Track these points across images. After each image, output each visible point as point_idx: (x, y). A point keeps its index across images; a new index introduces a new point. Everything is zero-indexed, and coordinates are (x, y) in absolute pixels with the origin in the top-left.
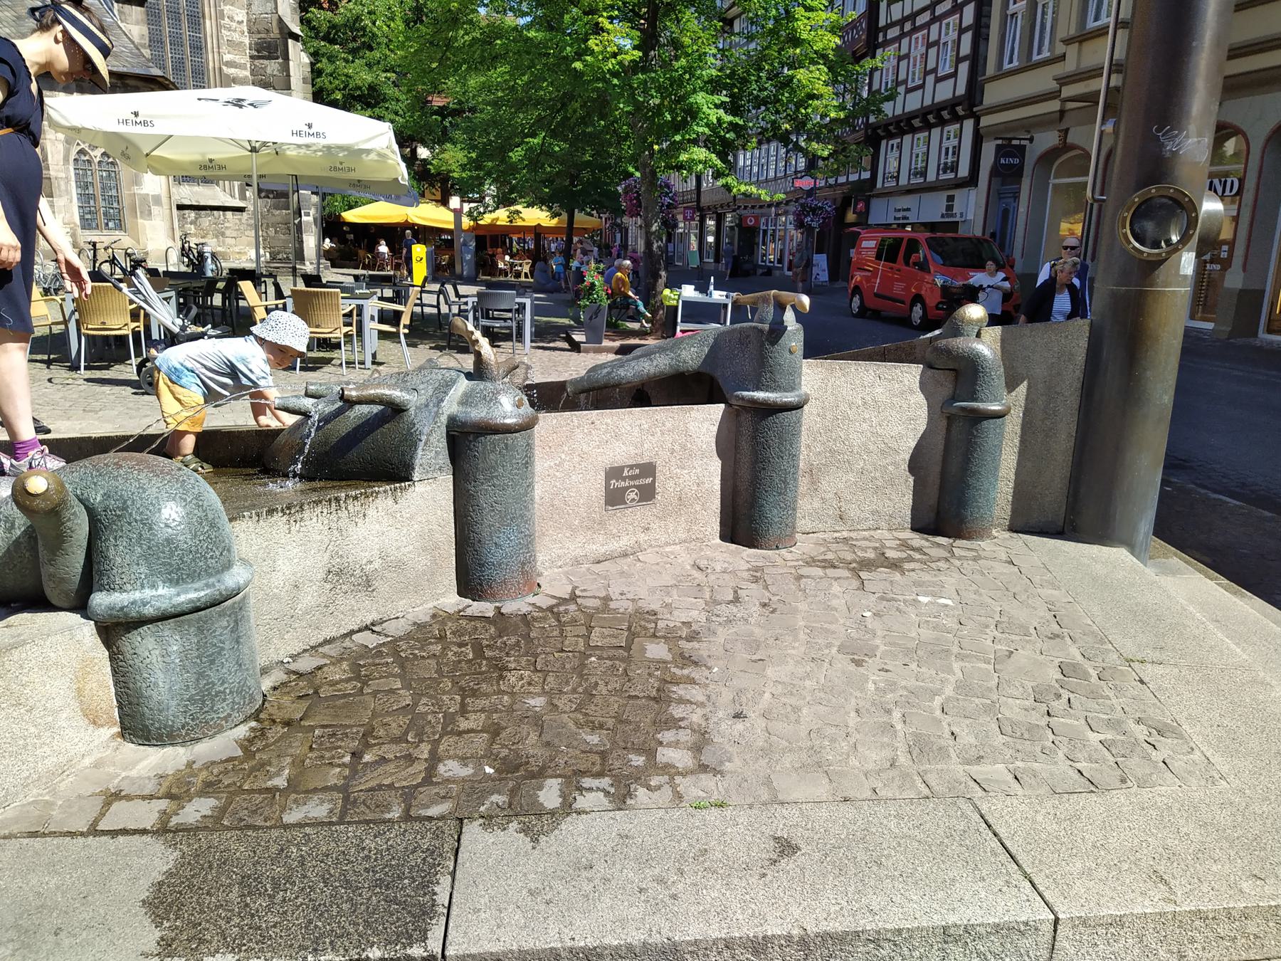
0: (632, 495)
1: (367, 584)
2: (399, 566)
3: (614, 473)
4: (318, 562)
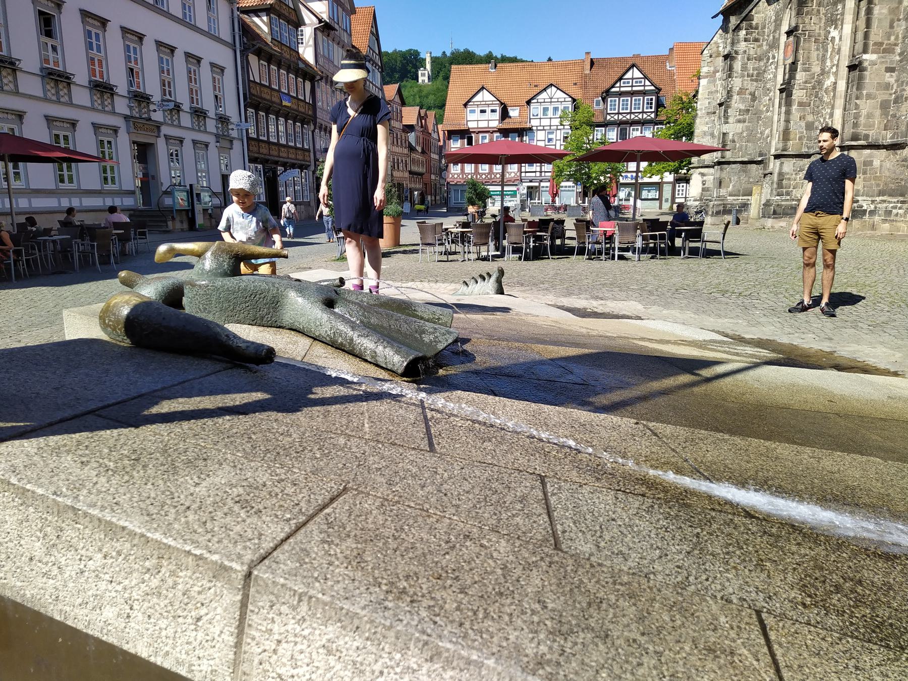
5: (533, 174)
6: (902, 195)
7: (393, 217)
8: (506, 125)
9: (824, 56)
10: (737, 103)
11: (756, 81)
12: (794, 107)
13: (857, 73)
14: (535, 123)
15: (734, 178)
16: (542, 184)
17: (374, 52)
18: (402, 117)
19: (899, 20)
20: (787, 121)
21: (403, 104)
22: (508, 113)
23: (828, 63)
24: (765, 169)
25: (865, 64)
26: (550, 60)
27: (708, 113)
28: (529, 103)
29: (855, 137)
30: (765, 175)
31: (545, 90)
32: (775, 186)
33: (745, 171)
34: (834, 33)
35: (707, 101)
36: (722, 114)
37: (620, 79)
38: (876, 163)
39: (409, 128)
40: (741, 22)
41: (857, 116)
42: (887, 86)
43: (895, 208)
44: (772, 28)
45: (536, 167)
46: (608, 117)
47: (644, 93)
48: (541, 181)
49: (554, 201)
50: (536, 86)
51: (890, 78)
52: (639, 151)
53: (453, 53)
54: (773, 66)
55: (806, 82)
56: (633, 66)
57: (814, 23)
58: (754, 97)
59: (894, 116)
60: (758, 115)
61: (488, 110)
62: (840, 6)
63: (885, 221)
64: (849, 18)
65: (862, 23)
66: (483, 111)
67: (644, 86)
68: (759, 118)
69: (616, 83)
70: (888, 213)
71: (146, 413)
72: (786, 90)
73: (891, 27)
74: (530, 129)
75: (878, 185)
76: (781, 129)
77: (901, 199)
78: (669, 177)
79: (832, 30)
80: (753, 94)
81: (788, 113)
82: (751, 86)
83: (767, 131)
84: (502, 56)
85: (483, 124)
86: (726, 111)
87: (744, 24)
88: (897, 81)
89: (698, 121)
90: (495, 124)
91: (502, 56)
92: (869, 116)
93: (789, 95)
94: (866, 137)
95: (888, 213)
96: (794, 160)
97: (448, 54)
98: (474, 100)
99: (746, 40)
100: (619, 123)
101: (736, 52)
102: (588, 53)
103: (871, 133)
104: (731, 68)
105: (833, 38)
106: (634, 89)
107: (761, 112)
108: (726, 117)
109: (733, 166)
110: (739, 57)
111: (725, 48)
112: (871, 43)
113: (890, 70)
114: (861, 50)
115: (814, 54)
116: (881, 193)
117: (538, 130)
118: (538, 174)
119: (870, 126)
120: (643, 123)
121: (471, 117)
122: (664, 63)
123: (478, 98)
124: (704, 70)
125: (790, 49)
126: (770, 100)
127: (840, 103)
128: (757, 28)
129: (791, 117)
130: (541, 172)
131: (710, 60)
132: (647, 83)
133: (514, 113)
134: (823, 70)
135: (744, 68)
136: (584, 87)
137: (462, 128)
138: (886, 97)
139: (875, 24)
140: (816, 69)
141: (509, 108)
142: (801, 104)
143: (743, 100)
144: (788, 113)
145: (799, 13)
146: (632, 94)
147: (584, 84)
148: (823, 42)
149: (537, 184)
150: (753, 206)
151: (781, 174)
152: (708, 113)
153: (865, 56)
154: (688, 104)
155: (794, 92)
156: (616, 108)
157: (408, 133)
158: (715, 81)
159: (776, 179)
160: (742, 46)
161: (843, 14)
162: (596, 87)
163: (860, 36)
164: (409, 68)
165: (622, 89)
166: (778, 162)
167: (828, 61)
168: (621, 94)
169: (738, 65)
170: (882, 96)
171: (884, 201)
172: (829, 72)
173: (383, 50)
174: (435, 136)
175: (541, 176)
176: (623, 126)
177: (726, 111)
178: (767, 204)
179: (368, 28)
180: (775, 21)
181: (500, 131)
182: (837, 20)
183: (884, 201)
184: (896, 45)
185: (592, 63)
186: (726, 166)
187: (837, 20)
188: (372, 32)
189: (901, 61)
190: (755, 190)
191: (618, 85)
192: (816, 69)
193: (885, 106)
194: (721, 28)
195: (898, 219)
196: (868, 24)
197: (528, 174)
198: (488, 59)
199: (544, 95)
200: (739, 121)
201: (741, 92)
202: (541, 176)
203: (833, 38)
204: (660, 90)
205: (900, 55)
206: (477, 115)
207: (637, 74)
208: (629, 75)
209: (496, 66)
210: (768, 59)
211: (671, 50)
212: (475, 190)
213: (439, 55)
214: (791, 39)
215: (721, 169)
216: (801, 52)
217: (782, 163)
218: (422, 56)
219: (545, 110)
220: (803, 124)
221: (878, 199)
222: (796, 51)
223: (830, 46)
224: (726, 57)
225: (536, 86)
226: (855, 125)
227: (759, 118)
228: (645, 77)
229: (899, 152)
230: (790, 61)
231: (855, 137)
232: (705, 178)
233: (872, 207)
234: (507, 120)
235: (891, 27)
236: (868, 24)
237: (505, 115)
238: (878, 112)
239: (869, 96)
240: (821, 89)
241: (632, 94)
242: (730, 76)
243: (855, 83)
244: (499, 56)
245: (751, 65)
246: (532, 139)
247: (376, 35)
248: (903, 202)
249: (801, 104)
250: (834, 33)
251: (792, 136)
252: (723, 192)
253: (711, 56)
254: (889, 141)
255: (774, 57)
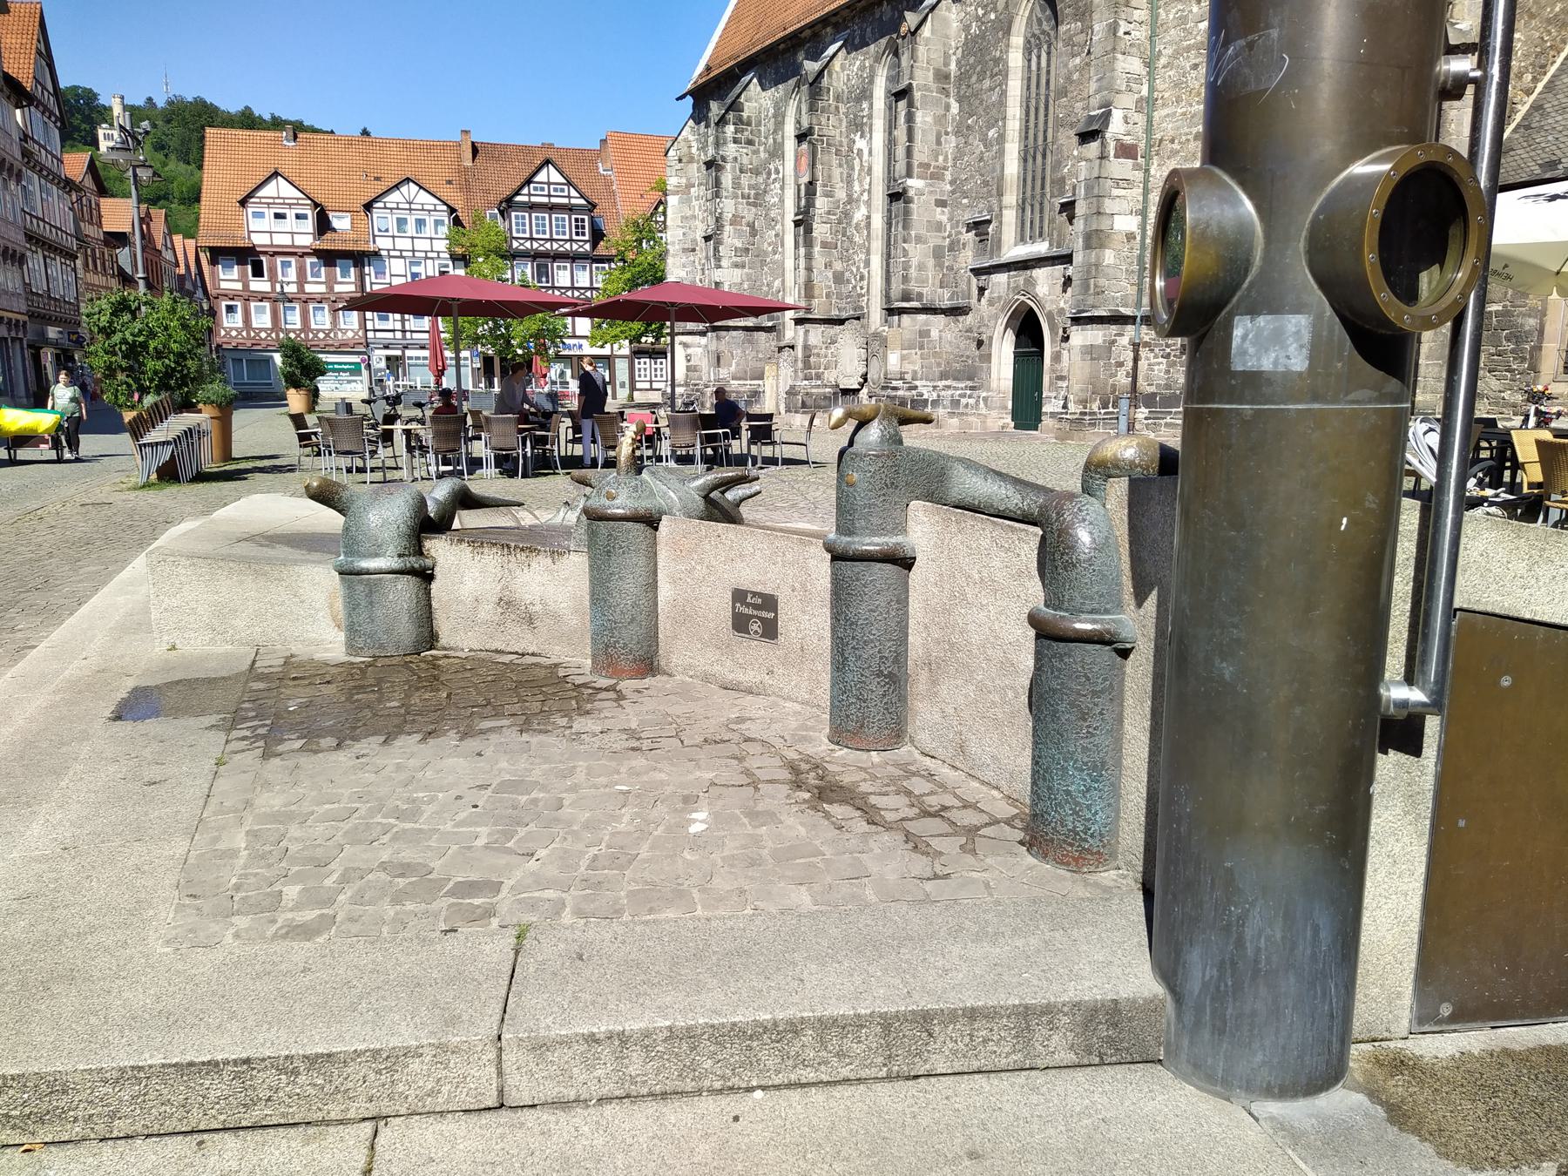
0: (755, 627)
1: (530, 620)
2: (556, 617)
3: (739, 595)
4: (492, 590)
5: (390, 335)
6: (971, 379)
7: (219, 406)
8: (326, 244)
9: (849, 176)
10: (731, 239)
11: (755, 205)
12: (817, 249)
13: (901, 204)
14: (383, 243)
15: (738, 352)
16: (408, 353)
17: (44, 88)
18: (100, 217)
19: (947, 133)
20: (809, 269)
21: (103, 191)
22: (329, 222)
23: (857, 187)
24: (779, 340)
25: (911, 193)
26: (365, 133)
27: (685, 250)
28: (368, 207)
29: (906, 297)
30: (780, 349)
31: (397, 187)
32: (800, 365)
33: (750, 342)
34: (860, 143)
35: (681, 232)
36: (711, 253)
37: (529, 182)
38: (934, 334)
39: (119, 239)
40: (727, 111)
41: (906, 267)
42: (939, 227)
43: (964, 396)
44: (771, 126)
45: (394, 321)
46: (515, 244)
47: (570, 209)
48: (406, 347)
49: (438, 383)
50: (377, 179)
51: (942, 215)
52: (673, 304)
53: (170, 103)
54: (777, 185)
55: (829, 213)
56: (547, 162)
57: (832, 126)
58: (754, 232)
59: (950, 268)
60: (761, 256)
61: (291, 214)
62: (865, 105)
63: (952, 414)
64: (879, 124)
65: (901, 133)
66: (278, 216)
67: (569, 197)
68: (763, 263)
69: (521, 188)
70: (955, 403)
71: (1155, 592)
72: (803, 222)
73: (939, 143)
74: (376, 254)
75: (939, 365)
76: (802, 280)
77: (970, 383)
78: (624, 348)
79: (857, 138)
80: (751, 226)
81: (809, 257)
82: (749, 214)
83: (777, 283)
84: (273, 117)
85: (282, 240)
86: (716, 249)
87: (731, 116)
88: (950, 220)
89: (670, 261)
90: (306, 241)
91: (273, 117)
92: (921, 267)
93: (809, 231)
94: (920, 296)
95: (955, 403)
96: (822, 327)
97: (161, 103)
98: (260, 194)
99: (735, 141)
100: (535, 256)
101: (724, 159)
102: (465, 132)
103: (925, 291)
104: (718, 183)
105: (860, 151)
106: (554, 200)
107: (766, 253)
108: (718, 259)
109: (734, 333)
110: (728, 166)
111: (703, 148)
112: (916, 163)
113: (941, 203)
114: (904, 173)
115: (836, 172)
116: (944, 376)
117: (390, 257)
118: (399, 335)
119: (923, 281)
120: (573, 258)
121: (255, 224)
122: (593, 162)
123: (269, 190)
124: (672, 182)
125: (805, 161)
126: (777, 235)
127: (877, 246)
128: (749, 124)
129: (814, 263)
130: (404, 331)
131: (679, 166)
132: (573, 193)
133: (341, 223)
134: (849, 196)
135: (737, 185)
136: (466, 188)
137: (241, 244)
138: (939, 242)
139: (918, 136)
140: (841, 195)
141: (331, 215)
142: (825, 245)
143: (739, 234)
144: (809, 257)
145: (812, 109)
146: (552, 208)
147: (465, 182)
148: (847, 155)
149: (398, 353)
150: (768, 394)
151: (806, 347)
152: (685, 250)
153: (910, 182)
154: (648, 229)
155: (815, 226)
156: (525, 230)
157: (115, 247)
158: (689, 200)
159: (800, 355)
160: (731, 150)
161: (870, 117)
162: (487, 192)
163: (900, 152)
164: (76, 122)
165: (534, 199)
166: (801, 329)
167: (856, 183)
168: (532, 207)
169: (727, 179)
170: (934, 240)
171: (949, 387)
172: (858, 200)
173: (63, 83)
174: (168, 255)
175: (404, 338)
176: (543, 260)
177: (716, 249)
178: (792, 392)
179: (31, 43)
180: (775, 116)
181: (318, 253)
182: (863, 124)
183: (949, 387)
184: (945, 168)
185: (475, 150)
186: (723, 333)
187: (863, 124)
188: (39, 52)
189: (953, 192)
190: (769, 370)
191: (525, 191)
192: (841, 195)
193: (938, 253)
194: (692, 117)
195: (968, 411)
196: (910, 138)
197: (379, 335)
198: (277, 124)
199: (395, 197)
200: (736, 266)
201: (736, 220)
202: (404, 338)
203: (860, 151)
204: (594, 206)
205: (951, 183)
206: (268, 222)
207: (556, 177)
208: (542, 177)
209: (295, 137)
210: (769, 174)
211: (604, 142)
212: (300, 360)
213: (140, 101)
214: (805, 146)
215: (718, 338)
216: (819, 167)
217: (807, 332)
218: (102, 101)
219: (401, 222)
220: (830, 275)
221: (941, 384)
222: (813, 165)
223: (857, 162)
224: (710, 164)
225: (377, 179)
226: (905, 279)
227: (763, 263)
228: (569, 183)
229: (961, 318)
230: (805, 179)
231: (906, 297)
232: (689, 351)
233: (935, 396)
234: (328, 235)
235: (939, 143)
236: (910, 138)
237: (323, 225)
238: (931, 262)
239: (919, 239)
240: (849, 224)
241: (552, 208)
242: (717, 195)
243: (900, 219)
244: (267, 117)
245: (745, 180)
246: (380, 273)
247: (46, 56)
248: (972, 388)
249: (825, 245)
250: (860, 143)
251: (817, 292)
252: (724, 373)
253: (680, 161)
254: (946, 304)
255: (777, 172)
